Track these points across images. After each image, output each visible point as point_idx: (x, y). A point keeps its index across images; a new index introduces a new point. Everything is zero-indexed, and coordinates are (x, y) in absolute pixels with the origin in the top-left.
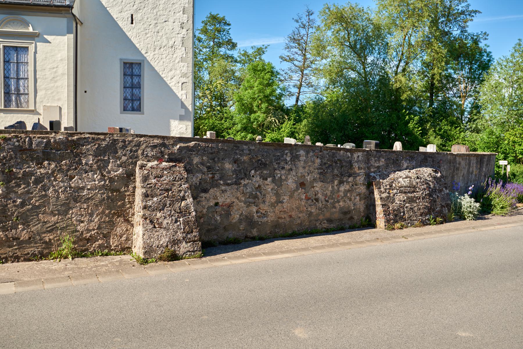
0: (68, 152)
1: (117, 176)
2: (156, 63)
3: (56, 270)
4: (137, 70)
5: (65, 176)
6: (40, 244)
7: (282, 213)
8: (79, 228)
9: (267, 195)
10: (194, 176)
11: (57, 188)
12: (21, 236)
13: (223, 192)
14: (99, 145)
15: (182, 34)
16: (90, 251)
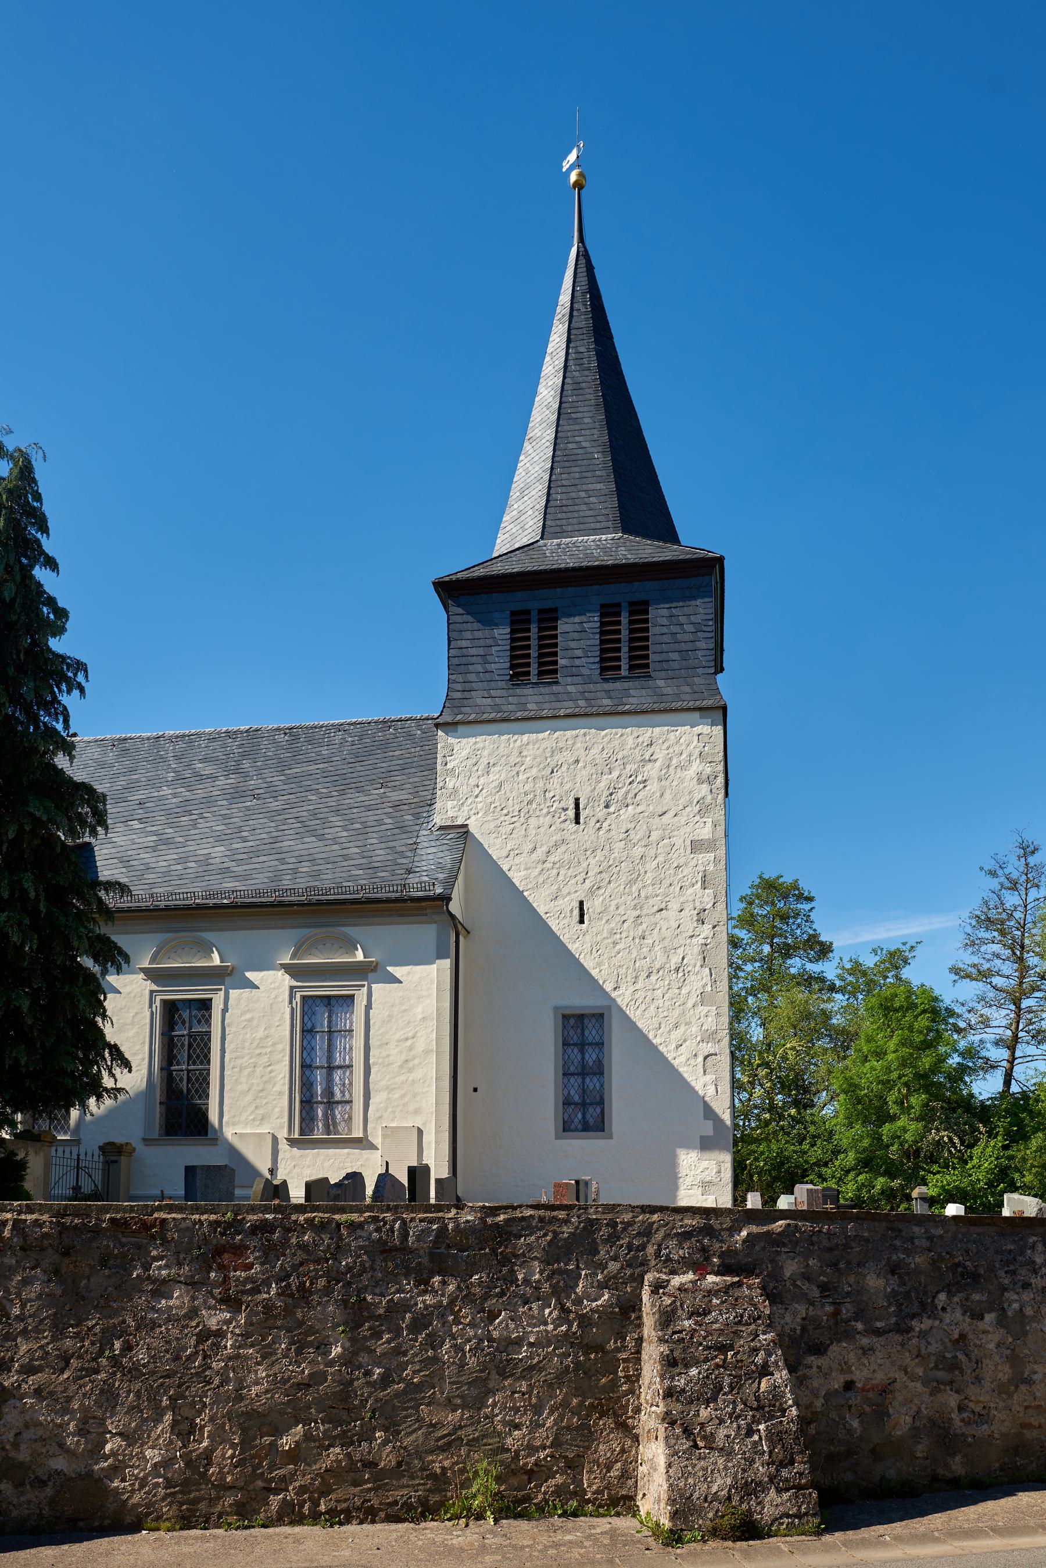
0: (485, 1254)
1: (597, 1311)
2: (639, 1012)
3: (462, 1550)
4: (594, 1032)
5: (479, 1313)
7: (1030, 1411)
8: (509, 1441)
9: (986, 1361)
10: (786, 1309)
11: (459, 1341)
12: (381, 1458)
13: (864, 1353)
14: (556, 1234)
15: (702, 936)
16: (535, 1501)
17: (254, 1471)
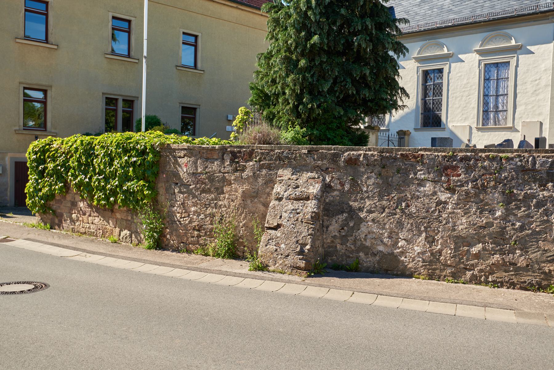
6: (539, 273)
12: (518, 262)
17: (460, 260)
